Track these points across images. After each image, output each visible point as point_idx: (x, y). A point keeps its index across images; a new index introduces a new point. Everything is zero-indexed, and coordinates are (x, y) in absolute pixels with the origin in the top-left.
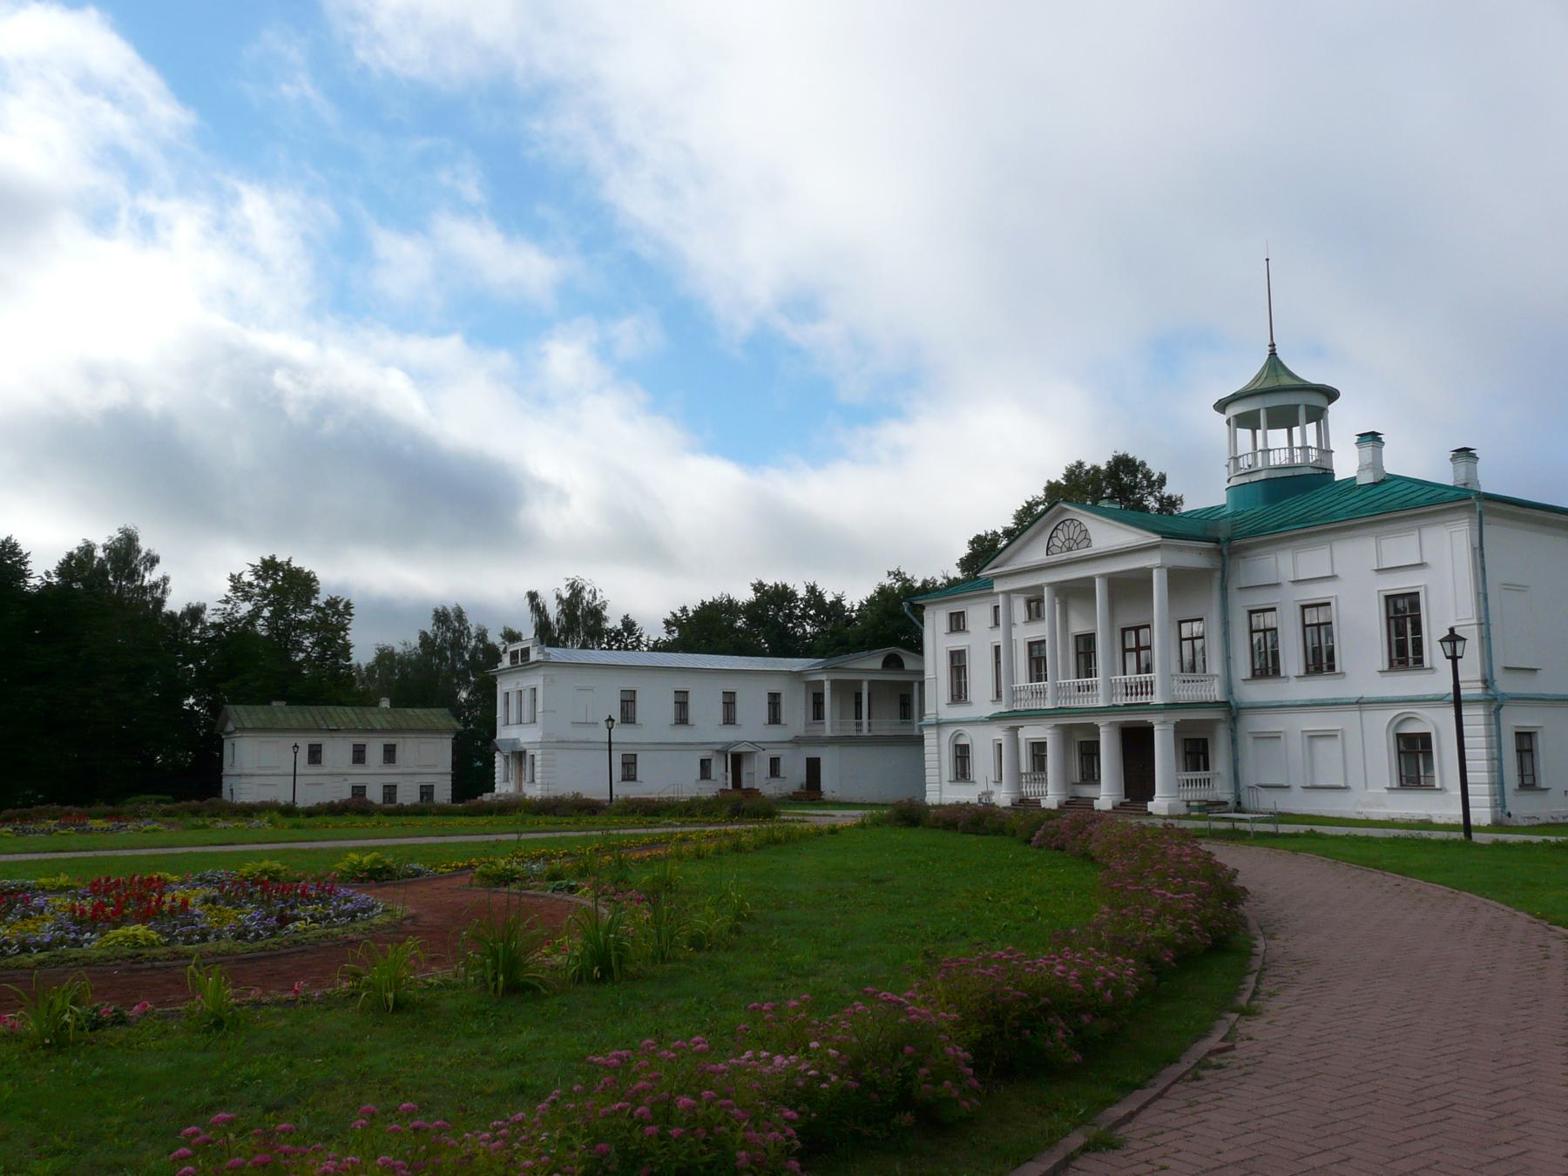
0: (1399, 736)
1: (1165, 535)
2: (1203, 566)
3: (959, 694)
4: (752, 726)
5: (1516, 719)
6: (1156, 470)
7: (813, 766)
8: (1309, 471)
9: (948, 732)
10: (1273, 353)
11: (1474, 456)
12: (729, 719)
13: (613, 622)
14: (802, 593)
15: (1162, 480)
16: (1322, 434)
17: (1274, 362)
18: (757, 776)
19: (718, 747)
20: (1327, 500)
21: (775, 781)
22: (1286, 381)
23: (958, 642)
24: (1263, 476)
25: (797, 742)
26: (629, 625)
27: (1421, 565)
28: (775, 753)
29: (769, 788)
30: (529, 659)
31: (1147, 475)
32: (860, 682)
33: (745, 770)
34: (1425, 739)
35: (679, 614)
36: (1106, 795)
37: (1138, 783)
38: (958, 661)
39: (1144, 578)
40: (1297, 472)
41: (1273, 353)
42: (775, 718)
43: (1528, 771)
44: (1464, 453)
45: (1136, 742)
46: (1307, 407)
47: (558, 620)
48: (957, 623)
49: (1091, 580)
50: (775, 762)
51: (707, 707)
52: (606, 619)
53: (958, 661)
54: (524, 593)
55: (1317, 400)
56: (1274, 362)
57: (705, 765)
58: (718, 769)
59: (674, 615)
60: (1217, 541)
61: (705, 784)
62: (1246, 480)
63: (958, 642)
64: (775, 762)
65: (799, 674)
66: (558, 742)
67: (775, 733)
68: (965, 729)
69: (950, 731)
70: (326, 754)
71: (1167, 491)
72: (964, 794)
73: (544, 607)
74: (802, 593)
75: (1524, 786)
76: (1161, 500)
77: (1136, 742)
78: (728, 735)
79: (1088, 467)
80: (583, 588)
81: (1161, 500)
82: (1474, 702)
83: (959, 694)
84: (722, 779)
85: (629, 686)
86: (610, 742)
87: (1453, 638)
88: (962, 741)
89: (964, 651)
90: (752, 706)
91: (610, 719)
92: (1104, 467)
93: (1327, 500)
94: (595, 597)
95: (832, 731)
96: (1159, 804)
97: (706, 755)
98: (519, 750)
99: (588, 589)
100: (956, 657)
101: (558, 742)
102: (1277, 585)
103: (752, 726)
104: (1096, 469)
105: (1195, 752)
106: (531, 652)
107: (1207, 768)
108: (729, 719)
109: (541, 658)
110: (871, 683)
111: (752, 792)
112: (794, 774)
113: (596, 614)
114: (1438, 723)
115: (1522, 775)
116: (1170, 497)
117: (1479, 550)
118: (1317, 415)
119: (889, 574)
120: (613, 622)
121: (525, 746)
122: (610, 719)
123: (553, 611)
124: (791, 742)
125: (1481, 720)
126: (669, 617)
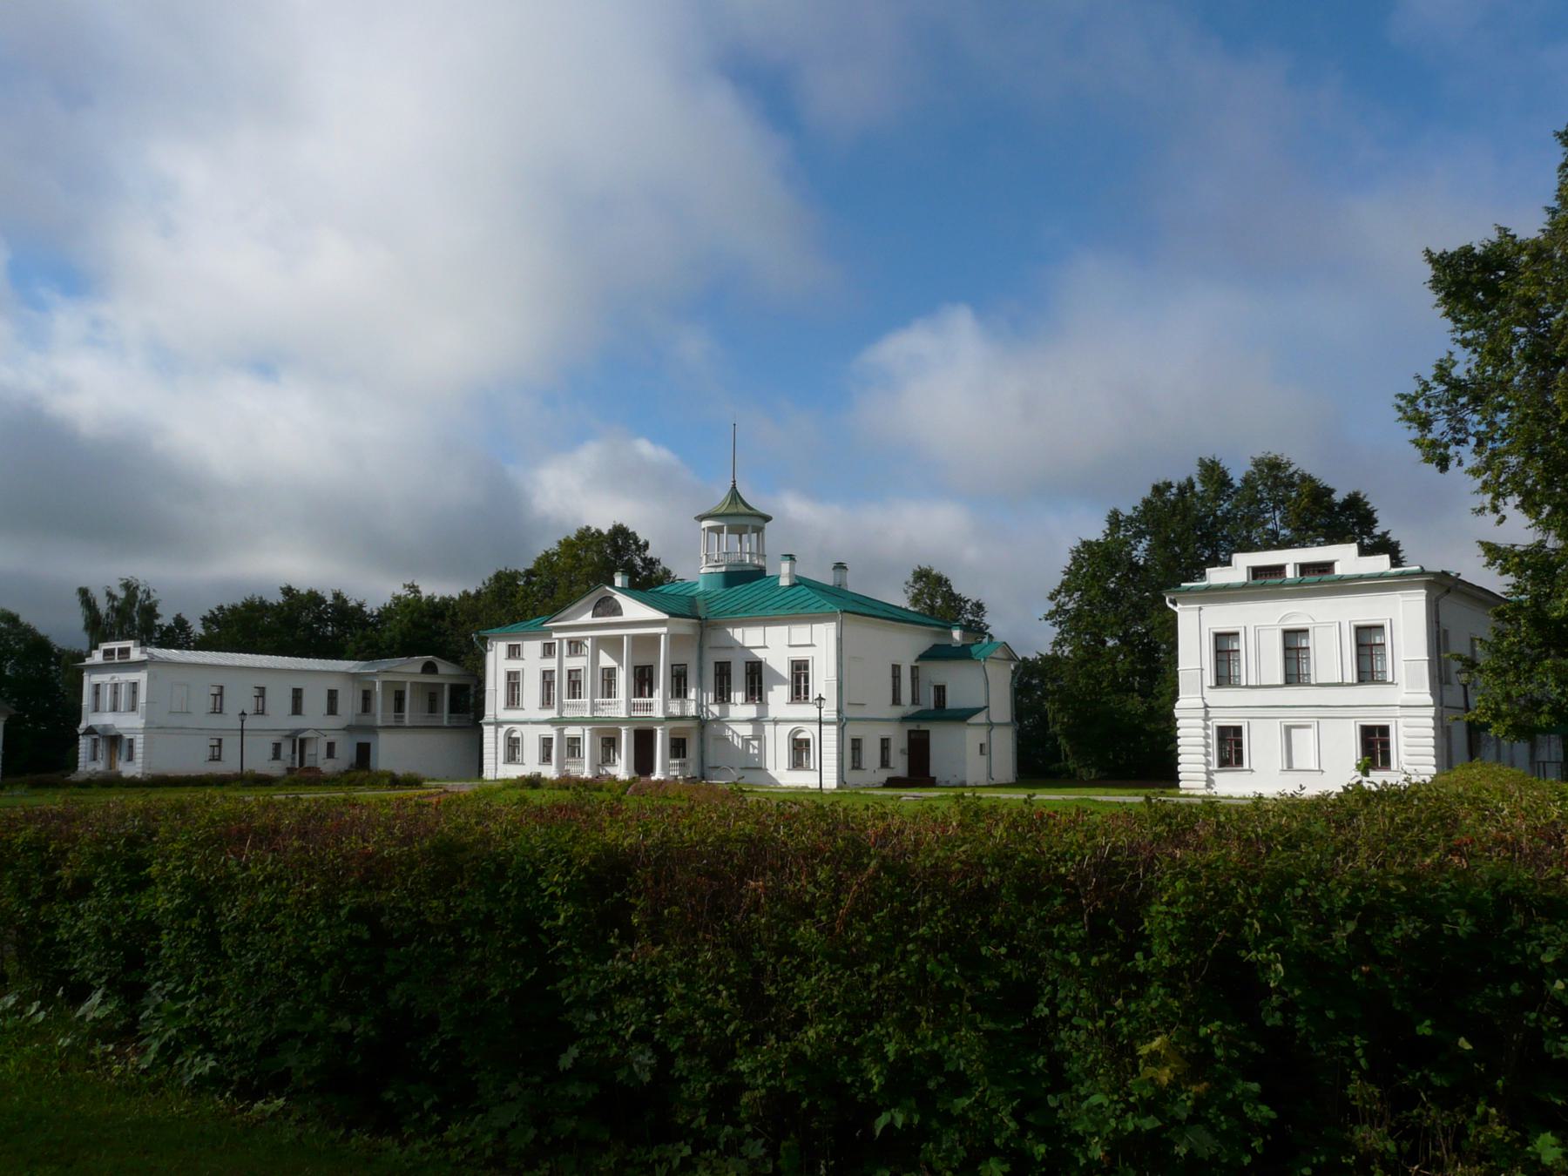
0: (794, 739)
1: (672, 615)
2: (688, 633)
3: (513, 700)
4: (314, 715)
5: (853, 731)
6: (642, 539)
7: (364, 752)
8: (751, 568)
9: (502, 731)
10: (734, 487)
11: (845, 568)
12: (297, 709)
13: (166, 619)
14: (329, 599)
15: (646, 545)
16: (760, 542)
17: (735, 495)
18: (317, 756)
19: (288, 733)
20: (762, 595)
21: (331, 762)
22: (742, 509)
23: (514, 665)
24: (723, 569)
25: (349, 729)
26: (181, 623)
27: (812, 645)
28: (331, 738)
29: (327, 767)
30: (129, 657)
31: (636, 541)
32: (405, 682)
33: (309, 750)
34: (807, 742)
35: (216, 613)
36: (621, 769)
37: (643, 762)
38: (513, 680)
39: (655, 638)
40: (745, 568)
41: (734, 487)
42: (332, 710)
43: (857, 759)
44: (840, 567)
45: (643, 740)
46: (753, 526)
47: (107, 615)
48: (514, 652)
49: (623, 636)
50: (331, 746)
51: (279, 702)
52: (157, 616)
53: (513, 680)
54: (75, 591)
55: (758, 522)
56: (735, 495)
57: (277, 747)
58: (286, 750)
59: (213, 613)
60: (699, 618)
61: (277, 764)
62: (713, 570)
63: (514, 665)
64: (331, 746)
65: (354, 676)
66: (158, 728)
67: (332, 722)
68: (516, 727)
69: (506, 727)
70: (1352, 749)
71: (649, 553)
72: (513, 772)
73: (94, 602)
74: (329, 599)
75: (854, 768)
76: (644, 560)
77: (643, 740)
78: (296, 723)
79: (593, 530)
80: (137, 587)
81: (644, 560)
82: (829, 723)
83: (513, 700)
84: (290, 760)
85: (297, 686)
86: (242, 730)
87: (820, 699)
88: (514, 735)
89: (519, 672)
90: (315, 702)
91: (243, 714)
92: (605, 532)
93: (762, 595)
94: (148, 596)
95: (449, 722)
96: (658, 775)
97: (276, 739)
98: (113, 734)
99: (142, 588)
100: (512, 676)
101: (158, 728)
102: (732, 648)
103: (314, 715)
104: (599, 532)
105: (678, 747)
106: (131, 651)
107: (684, 756)
108: (297, 709)
109: (145, 657)
110: (413, 684)
111: (315, 770)
112: (346, 754)
113: (150, 612)
114: (810, 732)
115: (853, 762)
116: (651, 559)
117: (840, 641)
118: (759, 530)
119: (405, 586)
120: (166, 619)
121: (121, 732)
122: (243, 714)
123: (103, 606)
124: (344, 729)
125: (835, 732)
126: (208, 614)
